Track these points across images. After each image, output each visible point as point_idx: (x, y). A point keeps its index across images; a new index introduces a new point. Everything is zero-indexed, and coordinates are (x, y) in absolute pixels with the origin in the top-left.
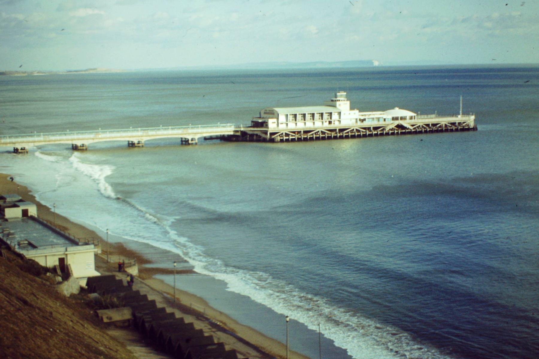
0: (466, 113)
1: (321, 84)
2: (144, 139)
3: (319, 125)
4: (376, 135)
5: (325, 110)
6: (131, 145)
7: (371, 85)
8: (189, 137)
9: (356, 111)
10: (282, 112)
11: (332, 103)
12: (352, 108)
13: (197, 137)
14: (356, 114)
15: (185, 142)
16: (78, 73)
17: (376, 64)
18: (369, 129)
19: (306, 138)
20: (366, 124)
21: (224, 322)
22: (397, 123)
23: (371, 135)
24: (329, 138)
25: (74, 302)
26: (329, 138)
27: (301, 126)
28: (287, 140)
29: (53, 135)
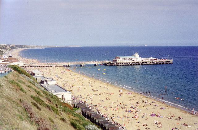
0: (171, 59)
1: (129, 51)
2: (84, 64)
3: (130, 61)
4: (146, 64)
5: (133, 57)
6: (81, 66)
7: (144, 51)
8: (96, 64)
9: (141, 58)
10: (121, 57)
11: (134, 56)
12: (139, 57)
13: (98, 64)
14: (141, 59)
15: (95, 65)
16: (65, 64)
17: (146, 45)
18: (144, 63)
19: (126, 65)
20: (143, 61)
21: (65, 65)
22: (152, 61)
23: (144, 64)
24: (133, 65)
25: (59, 109)
26: (133, 65)
27: (126, 61)
28: (122, 65)
29: (49, 62)
